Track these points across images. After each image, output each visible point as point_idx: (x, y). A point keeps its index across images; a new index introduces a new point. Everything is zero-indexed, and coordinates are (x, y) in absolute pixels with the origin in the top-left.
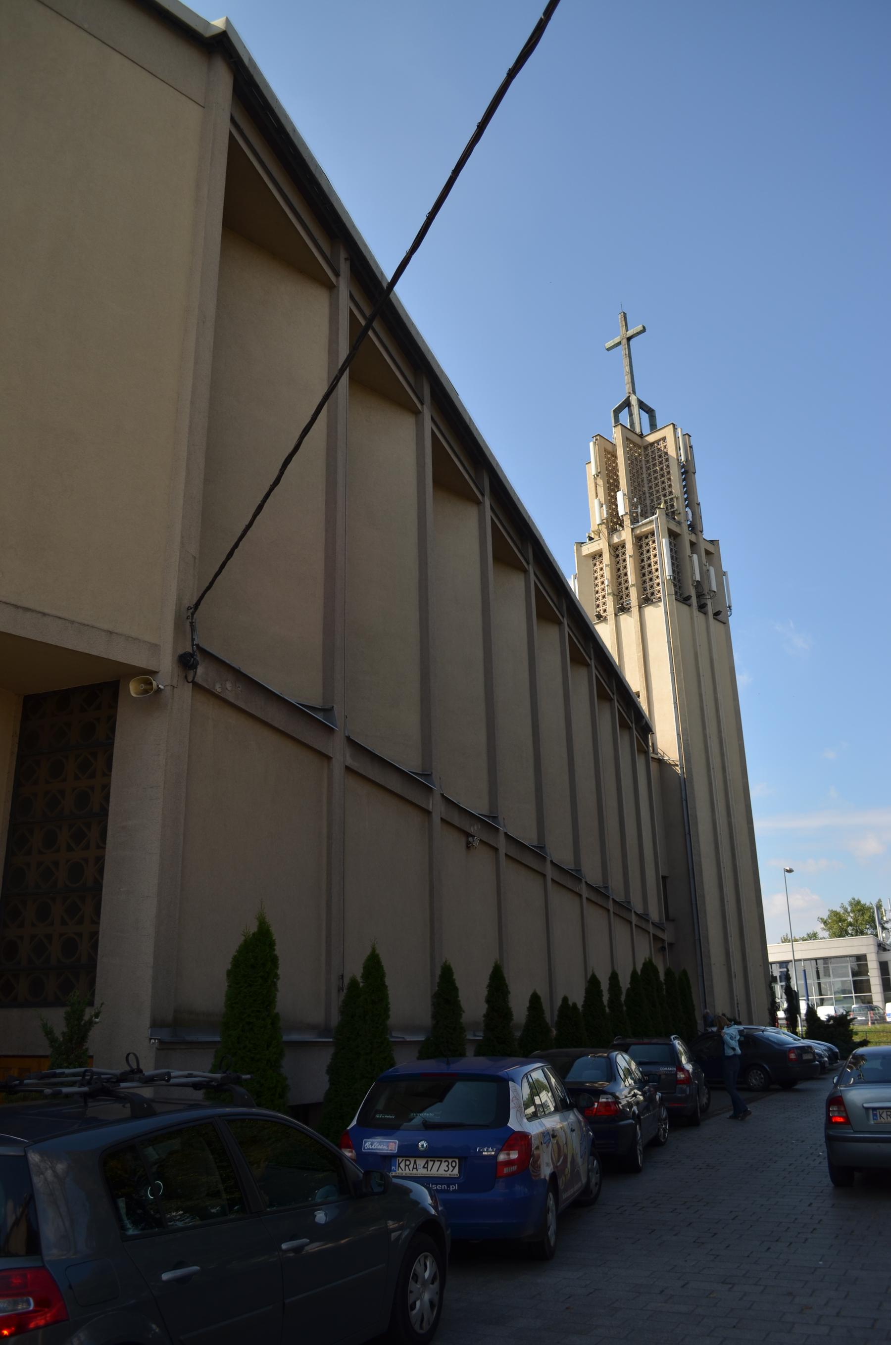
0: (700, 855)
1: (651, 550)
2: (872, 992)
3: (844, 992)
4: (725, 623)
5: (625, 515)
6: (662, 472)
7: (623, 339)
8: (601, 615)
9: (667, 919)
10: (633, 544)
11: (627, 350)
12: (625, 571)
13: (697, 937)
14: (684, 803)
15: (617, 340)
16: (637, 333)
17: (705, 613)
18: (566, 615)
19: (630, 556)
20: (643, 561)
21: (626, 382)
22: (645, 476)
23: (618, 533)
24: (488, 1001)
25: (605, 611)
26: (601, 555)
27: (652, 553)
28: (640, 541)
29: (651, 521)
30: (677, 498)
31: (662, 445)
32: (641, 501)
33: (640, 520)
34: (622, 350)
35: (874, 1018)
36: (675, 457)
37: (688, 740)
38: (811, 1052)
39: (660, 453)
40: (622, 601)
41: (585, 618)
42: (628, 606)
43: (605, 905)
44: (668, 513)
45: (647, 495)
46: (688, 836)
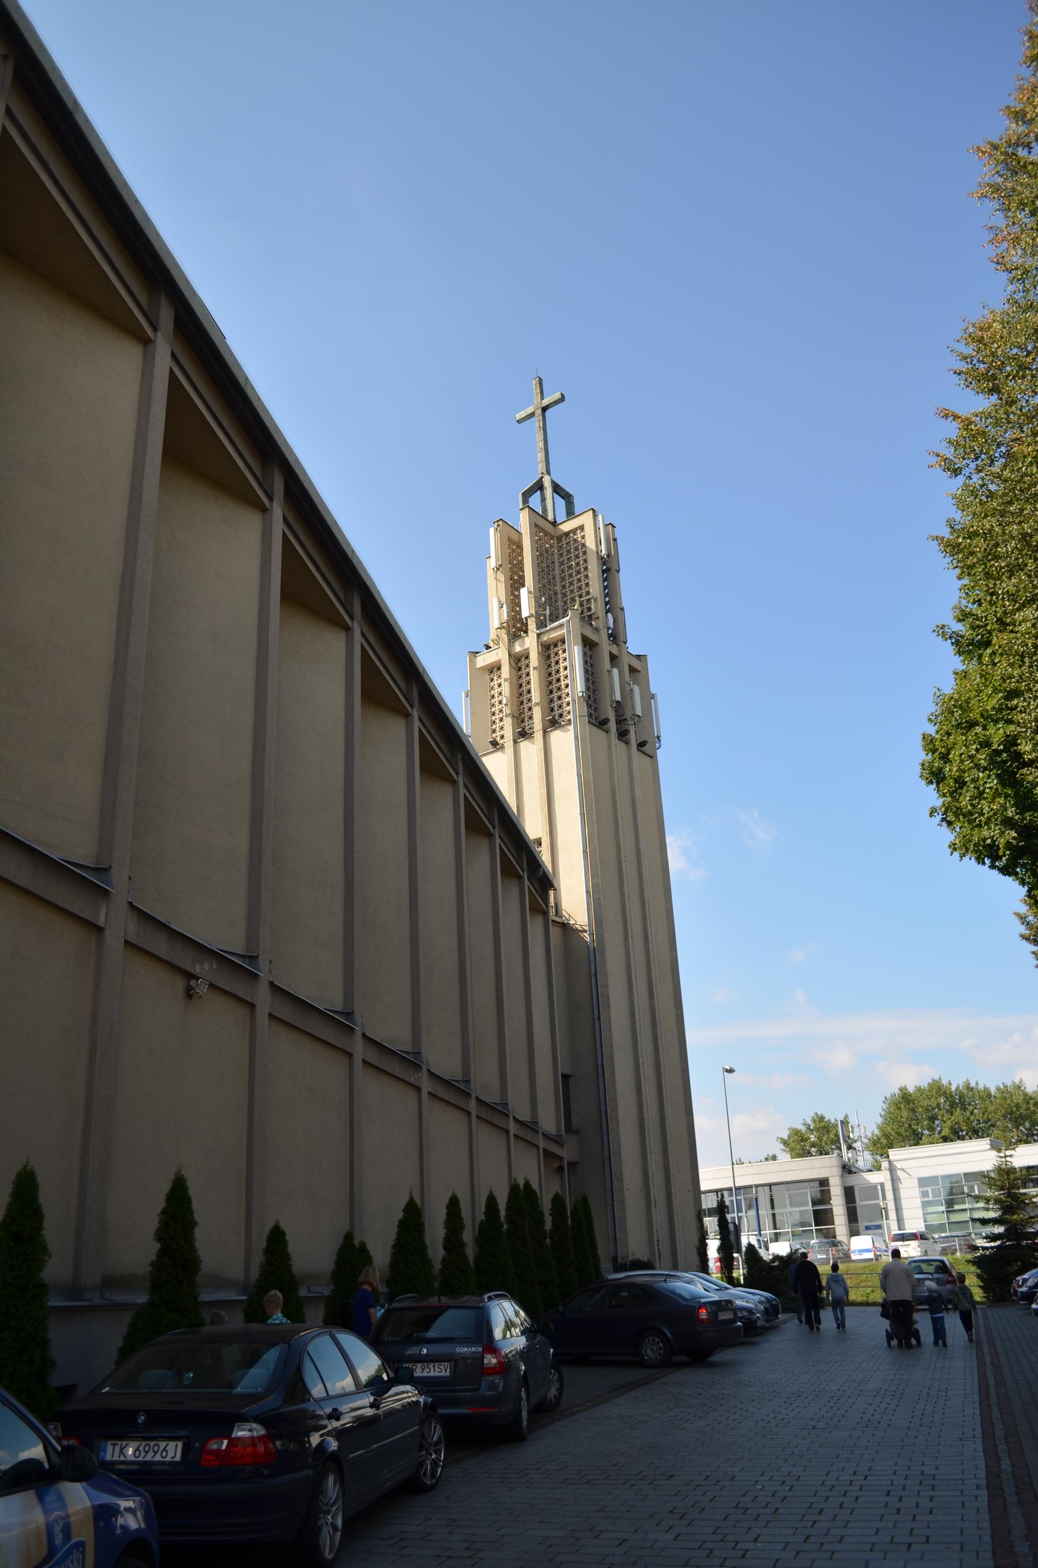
0: (611, 1047)
1: (561, 661)
2: (836, 1223)
3: (803, 1225)
4: (652, 757)
5: (529, 617)
6: (578, 568)
7: (537, 409)
8: (497, 742)
9: (569, 1129)
10: (538, 653)
11: (541, 422)
12: (528, 687)
13: (606, 1155)
14: (593, 979)
15: (530, 410)
16: (554, 402)
17: (627, 743)
18: (416, 704)
19: (534, 668)
20: (550, 674)
21: (539, 460)
22: (557, 572)
23: (520, 640)
24: (160, 1237)
25: (502, 737)
26: (499, 668)
27: (561, 665)
28: (548, 649)
29: (562, 625)
30: (595, 600)
31: (579, 535)
32: (551, 601)
33: (548, 624)
34: (536, 422)
35: (837, 1256)
36: (594, 549)
37: (600, 899)
38: (731, 1309)
39: (576, 545)
40: (523, 725)
41: (437, 697)
42: (531, 731)
43: (462, 1106)
44: (584, 617)
45: (560, 596)
46: (597, 1022)
